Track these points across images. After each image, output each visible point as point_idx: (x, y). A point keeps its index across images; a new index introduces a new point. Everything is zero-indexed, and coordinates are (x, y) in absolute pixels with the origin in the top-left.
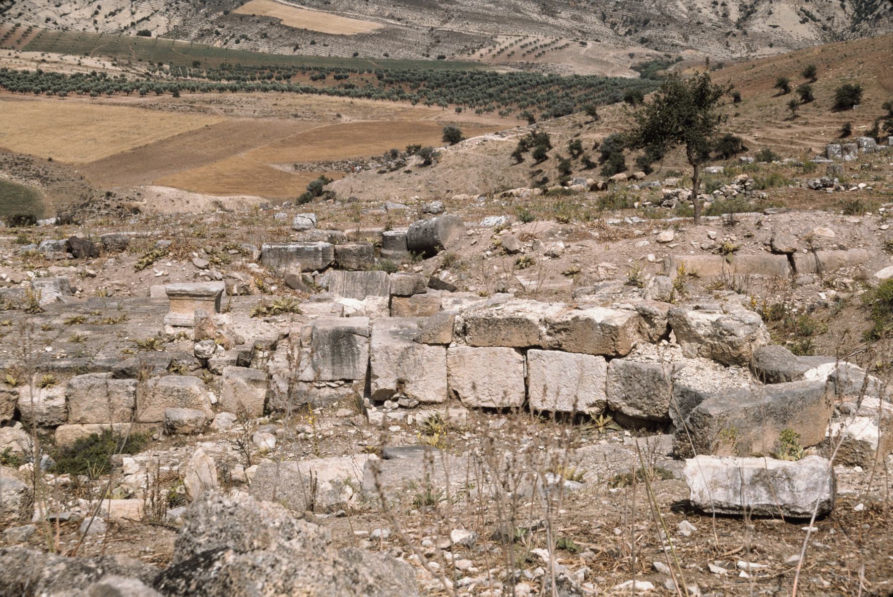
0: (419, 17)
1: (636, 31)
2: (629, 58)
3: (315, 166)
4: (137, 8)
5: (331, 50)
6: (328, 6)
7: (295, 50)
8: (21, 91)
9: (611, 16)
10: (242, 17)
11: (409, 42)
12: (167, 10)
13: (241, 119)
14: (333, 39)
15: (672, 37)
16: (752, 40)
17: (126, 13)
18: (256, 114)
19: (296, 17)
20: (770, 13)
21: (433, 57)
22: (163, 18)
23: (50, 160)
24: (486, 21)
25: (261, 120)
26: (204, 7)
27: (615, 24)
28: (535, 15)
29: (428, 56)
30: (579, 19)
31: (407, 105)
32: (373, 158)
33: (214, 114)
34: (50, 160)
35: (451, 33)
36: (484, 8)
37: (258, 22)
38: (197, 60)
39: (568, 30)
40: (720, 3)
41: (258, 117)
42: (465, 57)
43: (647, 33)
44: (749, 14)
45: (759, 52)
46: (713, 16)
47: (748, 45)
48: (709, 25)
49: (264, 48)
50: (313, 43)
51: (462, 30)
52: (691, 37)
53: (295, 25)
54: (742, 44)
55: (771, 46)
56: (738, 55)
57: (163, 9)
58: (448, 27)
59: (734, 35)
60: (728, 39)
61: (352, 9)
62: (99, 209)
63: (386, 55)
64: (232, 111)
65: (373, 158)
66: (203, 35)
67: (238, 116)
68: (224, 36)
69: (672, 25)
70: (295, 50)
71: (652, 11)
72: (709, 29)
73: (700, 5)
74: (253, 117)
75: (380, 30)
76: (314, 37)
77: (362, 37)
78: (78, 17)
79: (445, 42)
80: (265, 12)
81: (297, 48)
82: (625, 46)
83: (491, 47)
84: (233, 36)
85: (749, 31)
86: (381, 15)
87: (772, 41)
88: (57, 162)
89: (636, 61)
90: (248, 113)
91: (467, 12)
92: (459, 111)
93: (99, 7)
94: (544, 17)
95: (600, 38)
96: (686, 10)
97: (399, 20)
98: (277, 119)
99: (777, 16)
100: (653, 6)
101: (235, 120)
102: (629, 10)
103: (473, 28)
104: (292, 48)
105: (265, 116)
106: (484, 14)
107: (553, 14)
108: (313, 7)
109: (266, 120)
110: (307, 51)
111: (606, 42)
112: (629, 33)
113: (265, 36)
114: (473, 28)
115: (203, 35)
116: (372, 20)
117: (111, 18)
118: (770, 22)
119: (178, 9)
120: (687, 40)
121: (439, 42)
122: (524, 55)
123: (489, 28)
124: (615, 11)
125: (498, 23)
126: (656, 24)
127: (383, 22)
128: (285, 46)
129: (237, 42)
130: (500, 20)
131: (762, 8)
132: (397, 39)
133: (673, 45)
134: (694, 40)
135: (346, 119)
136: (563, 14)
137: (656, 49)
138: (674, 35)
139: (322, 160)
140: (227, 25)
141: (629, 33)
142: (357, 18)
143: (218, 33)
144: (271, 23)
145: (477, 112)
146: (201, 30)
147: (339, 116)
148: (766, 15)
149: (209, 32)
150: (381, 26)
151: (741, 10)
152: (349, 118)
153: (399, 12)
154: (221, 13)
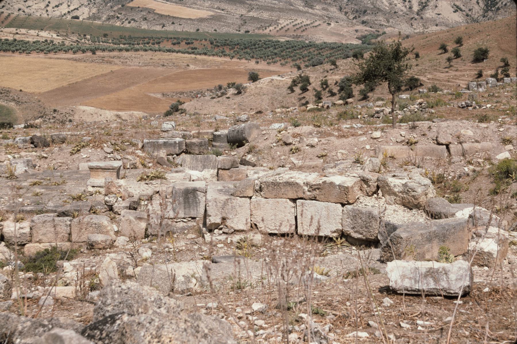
0: (234, 8)
1: (359, 17)
2: (355, 33)
3: (174, 94)
4: (71, 3)
5: (184, 27)
7: (163, 27)
8: (4, 51)
10: (132, 8)
11: (229, 23)
13: (131, 67)
18: (140, 64)
19: (163, 8)
20: (436, 7)
21: (242, 32)
24: (273, 11)
25: (143, 68)
27: (347, 13)
28: (301, 7)
29: (239, 31)
30: (327, 10)
31: (227, 59)
32: (208, 90)
33: (116, 64)
35: (253, 18)
36: (271, 3)
37: (141, 11)
38: (106, 33)
39: (320, 16)
41: (141, 66)
42: (261, 32)
43: (365, 18)
44: (424, 7)
45: (430, 29)
46: (403, 8)
47: (423, 25)
48: (401, 13)
50: (173, 23)
52: (391, 20)
53: (163, 13)
54: (420, 24)
55: (437, 25)
56: (418, 31)
58: (251, 14)
59: (416, 19)
60: (412, 22)
61: (196, 4)
63: (215, 30)
64: (126, 62)
65: (208, 90)
66: (109, 19)
68: (122, 19)
69: (380, 13)
70: (163, 27)
72: (401, 15)
74: (139, 66)
75: (212, 16)
76: (174, 20)
80: (145, 5)
81: (164, 26)
82: (353, 25)
83: (276, 26)
84: (127, 19)
85: (424, 17)
86: (212, 7)
89: (359, 34)
92: (257, 63)
94: (306, 8)
95: (339, 21)
96: (388, 5)
97: (223, 10)
99: (440, 8)
102: (355, 5)
103: (265, 15)
104: (161, 26)
105: (146, 66)
106: (272, 7)
107: (312, 7)
109: (146, 68)
110: (170, 28)
112: (355, 18)
114: (265, 15)
115: (109, 19)
116: (207, 10)
117: (56, 9)
118: (436, 11)
119: (95, 3)
120: (388, 22)
121: (246, 23)
122: (295, 30)
123: (275, 15)
124: (347, 5)
125: (280, 12)
126: (371, 13)
127: (214, 11)
128: (157, 25)
130: (281, 10)
134: (392, 22)
135: (192, 67)
137: (371, 27)
140: (123, 13)
141: (355, 18)
142: (198, 9)
143: (118, 18)
147: (188, 65)
148: (434, 7)
149: (113, 17)
151: (419, 5)
154: (120, 6)
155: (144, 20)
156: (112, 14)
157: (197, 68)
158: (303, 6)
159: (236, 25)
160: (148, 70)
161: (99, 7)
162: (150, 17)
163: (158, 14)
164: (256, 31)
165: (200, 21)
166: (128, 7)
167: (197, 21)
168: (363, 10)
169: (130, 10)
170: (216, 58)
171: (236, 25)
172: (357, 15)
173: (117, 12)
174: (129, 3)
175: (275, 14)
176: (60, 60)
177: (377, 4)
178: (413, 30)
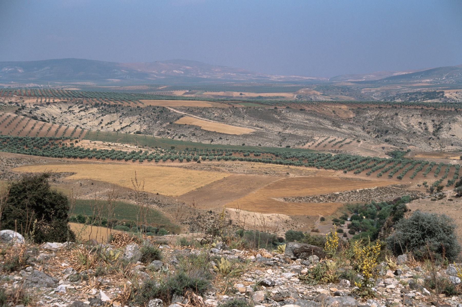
0: (271, 126)
1: (381, 136)
2: (382, 149)
3: (294, 199)
4: (123, 121)
5: (230, 142)
6: (223, 120)
7: (211, 142)
8: (118, 160)
9: (367, 128)
10: (180, 125)
11: (270, 139)
12: (139, 122)
13: (239, 175)
14: (231, 136)
15: (401, 139)
16: (442, 142)
17: (117, 123)
18: (245, 172)
19: (208, 125)
20: (450, 129)
21: (284, 146)
22: (137, 125)
23: (158, 194)
24: (307, 129)
25: (249, 175)
26: (159, 120)
27: (370, 132)
28: (330, 127)
29: (281, 146)
30: (352, 129)
31: (314, 169)
32: (321, 196)
33: (224, 172)
34: (158, 194)
35: (290, 135)
36: (303, 123)
37: (189, 128)
38: (173, 146)
39: (348, 135)
40: (423, 123)
41: (246, 174)
42: (300, 147)
43: (388, 137)
44: (439, 129)
45: (446, 148)
46: (420, 129)
47: (440, 145)
48: (419, 134)
49: (195, 140)
50: (221, 138)
51: (295, 133)
52: (411, 140)
53: (209, 130)
54: (437, 144)
55: (452, 145)
56: (436, 149)
57: (137, 121)
58: (287, 131)
59: (433, 139)
60: (430, 141)
61: (236, 122)
62: (209, 219)
63: (260, 145)
64: (232, 170)
65: (321, 196)
66: (160, 134)
67: (237, 173)
68: (172, 135)
69: (400, 133)
70: (211, 142)
71: (389, 126)
72: (420, 135)
73: (412, 124)
74: (244, 173)
75: (254, 132)
76: (221, 136)
77: (246, 136)
78: (92, 125)
79: (289, 139)
80: (191, 123)
81: (212, 141)
82: (379, 143)
83: (313, 142)
84: (177, 135)
85: (440, 137)
86: (251, 125)
87: (453, 143)
88: (162, 195)
89: (386, 150)
90: (241, 171)
91: (295, 124)
92: (345, 172)
93: (102, 120)
94: (334, 128)
95: (366, 139)
96: (406, 126)
97: (261, 128)
98: (257, 175)
99: (454, 130)
100: (388, 123)
101: (236, 175)
102: (376, 125)
103: (300, 133)
104: (210, 141)
105: (251, 173)
106: (304, 126)
107: (339, 126)
108: (216, 120)
109: (252, 175)
110: (217, 142)
111: (369, 141)
112: (377, 137)
113: (194, 135)
114: (300, 133)
115: (160, 134)
116: (248, 128)
117: (109, 126)
118: (450, 133)
119: (145, 121)
120: (409, 141)
121: (285, 139)
122: (332, 146)
123: (309, 133)
124: (369, 125)
125: (313, 130)
126: (392, 133)
127: (255, 129)
128: (206, 140)
129: (180, 138)
130: (313, 128)
131: (445, 126)
132: (264, 137)
133: (403, 143)
134: (413, 141)
135: (291, 175)
136: (344, 127)
137: (394, 145)
138: (402, 138)
139: (296, 196)
140: (173, 129)
141: (377, 137)
142: (240, 126)
143: (168, 133)
144: (196, 129)
145: (354, 173)
146: (159, 132)
147: (288, 174)
148: (448, 129)
149: (163, 133)
150: (253, 130)
151: (434, 127)
152: (293, 175)
153: (261, 124)
154: (168, 123)
155: (193, 136)
156: (162, 130)
157: (297, 176)
158: (331, 126)
159: (277, 140)
160: (254, 177)
161: (149, 124)
162: (197, 132)
163: (205, 130)
164: (296, 146)
165: (244, 137)
166: (176, 124)
167: (242, 137)
168: (385, 130)
169: (178, 127)
170: (308, 169)
171: (277, 140)
172: (379, 134)
173: (167, 128)
174: (176, 120)
175: (308, 132)
176: (172, 168)
177: (396, 125)
178: (431, 148)
